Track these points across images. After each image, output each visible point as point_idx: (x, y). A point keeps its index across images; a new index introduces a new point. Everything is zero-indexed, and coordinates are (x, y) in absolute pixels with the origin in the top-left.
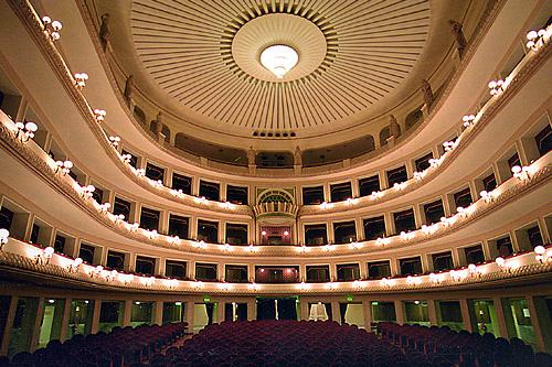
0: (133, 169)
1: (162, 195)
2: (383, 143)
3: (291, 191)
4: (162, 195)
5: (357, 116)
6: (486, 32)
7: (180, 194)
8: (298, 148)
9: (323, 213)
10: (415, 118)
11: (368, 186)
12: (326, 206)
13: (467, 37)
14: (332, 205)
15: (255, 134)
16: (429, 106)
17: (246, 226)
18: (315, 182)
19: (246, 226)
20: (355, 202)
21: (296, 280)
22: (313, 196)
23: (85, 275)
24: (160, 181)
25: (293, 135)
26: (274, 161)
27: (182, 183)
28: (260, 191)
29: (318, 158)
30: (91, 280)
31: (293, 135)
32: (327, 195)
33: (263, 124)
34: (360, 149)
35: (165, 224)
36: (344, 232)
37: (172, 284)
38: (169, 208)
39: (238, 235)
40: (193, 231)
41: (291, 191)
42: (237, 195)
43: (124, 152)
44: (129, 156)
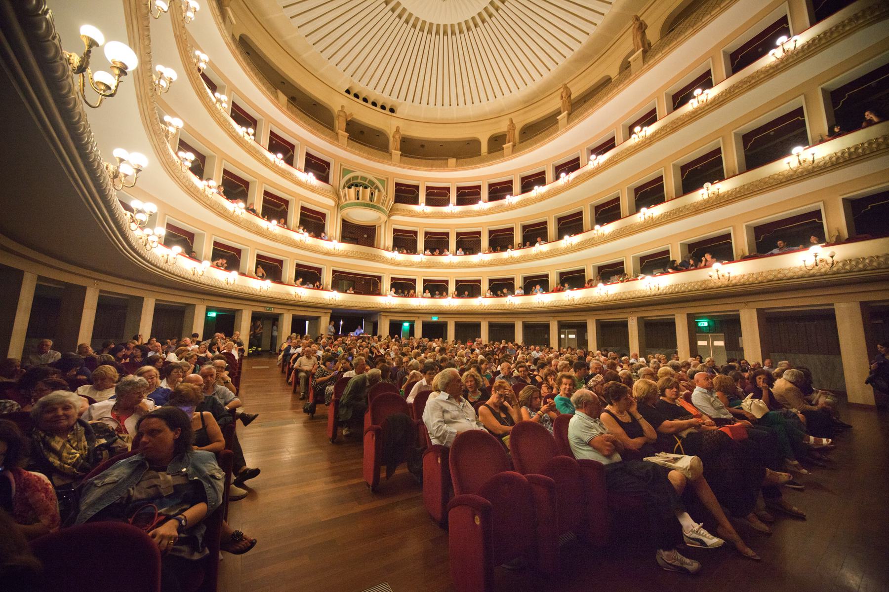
0: (194, 179)
1: (302, 187)
2: (490, 151)
3: (382, 182)
4: (268, 173)
5: (471, 110)
6: (693, 34)
7: (273, 226)
8: (398, 130)
9: (328, 254)
10: (534, 131)
11: (468, 195)
12: (422, 207)
13: (653, 35)
14: (430, 209)
15: (348, 91)
16: (569, 114)
17: (323, 215)
18: (441, 180)
19: (323, 215)
20: (824, 151)
21: (377, 292)
22: (406, 194)
23: (114, 469)
24: (251, 131)
25: (392, 110)
26: (362, 136)
27: (280, 145)
29: (415, 150)
30: (165, 266)
31: (392, 110)
32: (453, 197)
33: (366, 80)
34: (465, 151)
36: (437, 243)
37: (304, 293)
38: (265, 181)
39: (313, 222)
40: (294, 216)
41: (382, 182)
42: (318, 166)
43: (184, 146)
44: (191, 156)
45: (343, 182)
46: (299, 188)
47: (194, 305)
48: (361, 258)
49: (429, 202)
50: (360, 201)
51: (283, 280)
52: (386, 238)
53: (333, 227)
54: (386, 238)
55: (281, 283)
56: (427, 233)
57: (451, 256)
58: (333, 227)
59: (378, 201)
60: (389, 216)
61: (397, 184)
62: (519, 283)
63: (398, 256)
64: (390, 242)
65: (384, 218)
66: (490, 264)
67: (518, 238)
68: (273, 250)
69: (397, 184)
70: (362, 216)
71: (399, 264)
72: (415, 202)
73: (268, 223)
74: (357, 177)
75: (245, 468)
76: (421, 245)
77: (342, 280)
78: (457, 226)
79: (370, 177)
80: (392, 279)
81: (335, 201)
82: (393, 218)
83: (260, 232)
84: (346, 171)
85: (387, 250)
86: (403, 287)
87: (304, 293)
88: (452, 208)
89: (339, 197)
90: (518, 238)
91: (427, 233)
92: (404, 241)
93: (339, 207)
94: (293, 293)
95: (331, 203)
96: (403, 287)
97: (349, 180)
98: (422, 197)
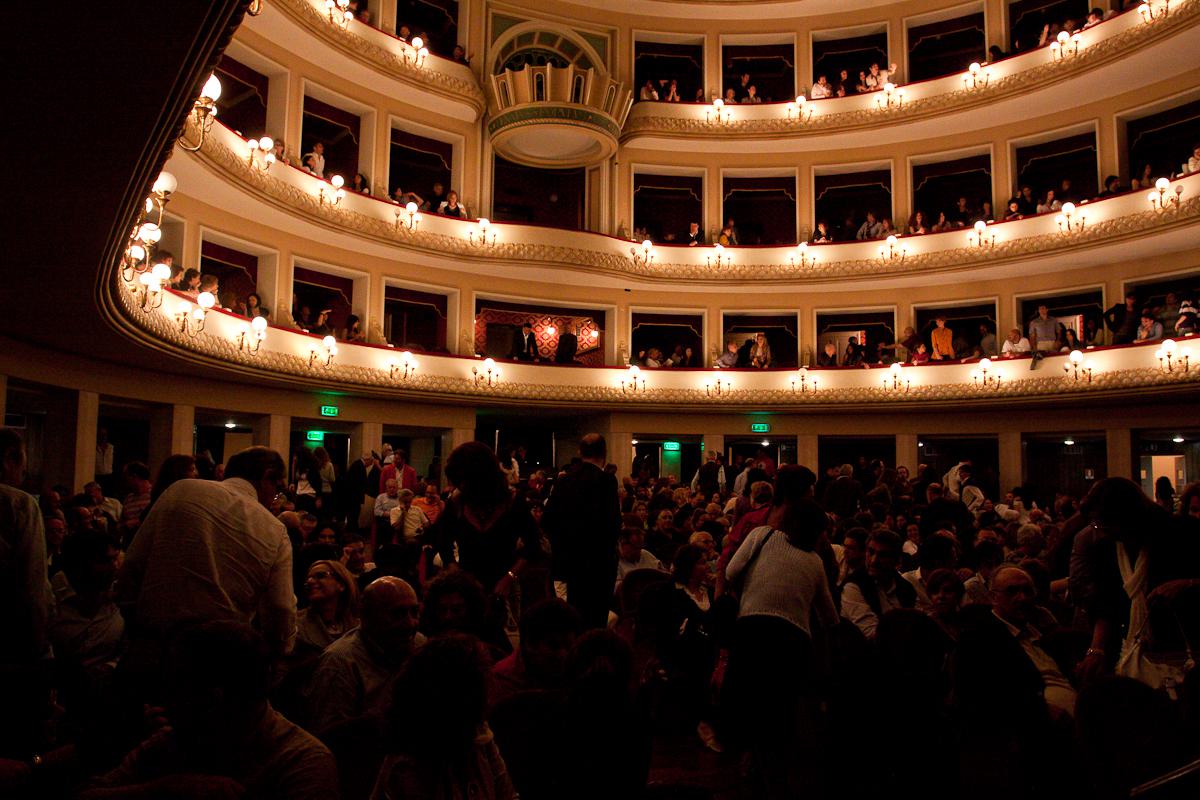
3: (599, 43)
17: (446, 149)
19: (446, 149)
28: (501, 23)
35: (373, 312)
41: (599, 43)
45: (493, 56)
46: (387, 80)
47: (269, 415)
48: (563, 265)
49: (736, 93)
50: (548, 103)
51: (449, 345)
52: (616, 202)
53: (473, 178)
54: (616, 202)
55: (445, 352)
56: (729, 183)
57: (803, 246)
58: (473, 178)
59: (595, 101)
60: (623, 140)
61: (641, 47)
62: (1007, 316)
63: (651, 254)
64: (624, 213)
65: (609, 143)
66: (920, 267)
67: (1002, 183)
68: (333, 253)
69: (641, 47)
70: (546, 144)
71: (654, 276)
72: (693, 93)
73: (323, 184)
74: (528, 37)
75: (1071, 710)
76: (713, 212)
77: (505, 333)
78: (1127, 263)
79: (565, 31)
80: (637, 317)
81: (478, 109)
82: (635, 144)
83: (308, 211)
84: (501, 23)
85: (621, 236)
86: (667, 339)
87: (319, 352)
88: (809, 106)
89: (488, 97)
90: (1002, 183)
91: (729, 183)
92: (667, 211)
93: (488, 123)
94: (470, 376)
95: (468, 113)
96: (667, 339)
97: (510, 46)
98: (713, 77)
